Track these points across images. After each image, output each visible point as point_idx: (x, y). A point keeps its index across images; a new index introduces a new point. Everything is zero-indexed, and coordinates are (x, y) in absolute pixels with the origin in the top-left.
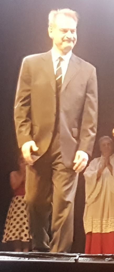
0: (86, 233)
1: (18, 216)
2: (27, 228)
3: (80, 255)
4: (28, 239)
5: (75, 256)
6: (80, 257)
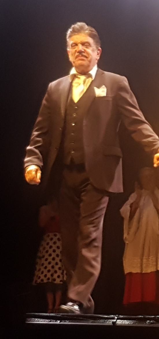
0: (126, 273)
1: (49, 263)
2: (60, 269)
3: (118, 317)
4: (61, 281)
5: (113, 318)
6: (118, 319)
